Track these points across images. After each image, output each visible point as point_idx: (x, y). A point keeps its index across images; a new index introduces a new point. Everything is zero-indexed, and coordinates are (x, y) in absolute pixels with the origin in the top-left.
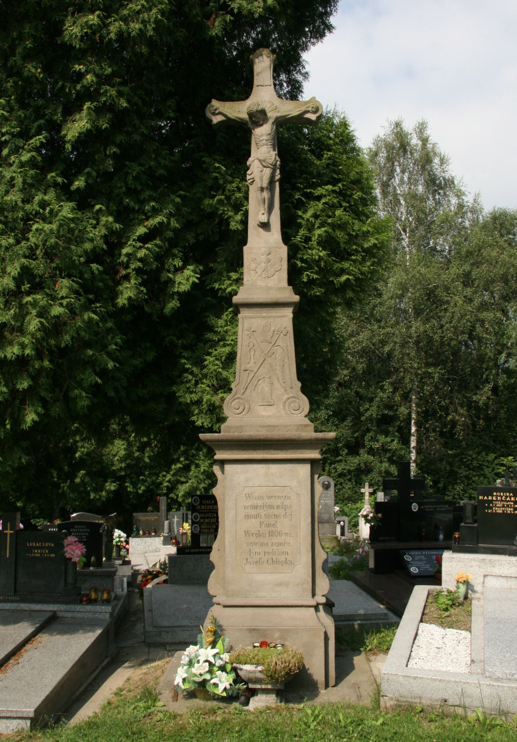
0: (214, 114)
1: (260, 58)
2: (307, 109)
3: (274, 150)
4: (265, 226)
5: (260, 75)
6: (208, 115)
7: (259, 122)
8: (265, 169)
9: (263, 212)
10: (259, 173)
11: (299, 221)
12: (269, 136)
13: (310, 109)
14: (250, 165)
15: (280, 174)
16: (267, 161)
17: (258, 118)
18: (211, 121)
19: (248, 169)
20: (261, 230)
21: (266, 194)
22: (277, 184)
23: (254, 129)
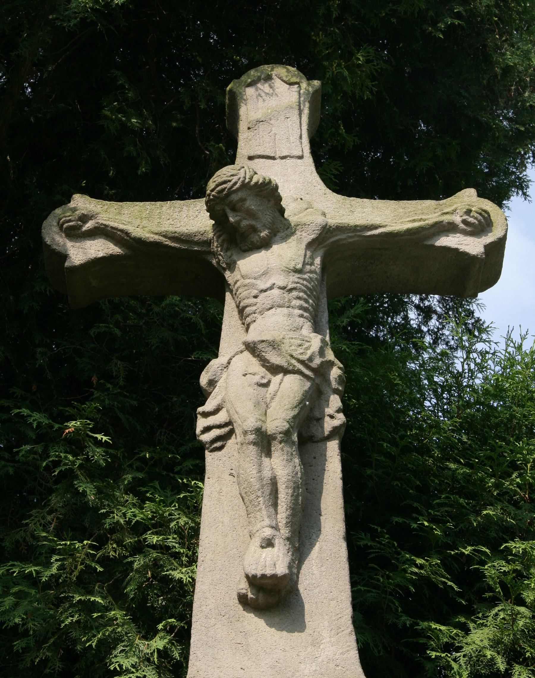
0: (75, 233)
1: (265, 87)
2: (446, 219)
3: (317, 329)
4: (274, 599)
5: (262, 127)
6: (53, 236)
7: (255, 230)
8: (276, 379)
9: (268, 532)
10: (253, 391)
11: (400, 627)
12: (295, 277)
13: (457, 219)
14: (212, 383)
15: (345, 410)
16: (285, 347)
17: (251, 215)
18: (64, 257)
19: (202, 396)
20: (255, 623)
21: (282, 465)
22: (333, 448)
23: (231, 266)
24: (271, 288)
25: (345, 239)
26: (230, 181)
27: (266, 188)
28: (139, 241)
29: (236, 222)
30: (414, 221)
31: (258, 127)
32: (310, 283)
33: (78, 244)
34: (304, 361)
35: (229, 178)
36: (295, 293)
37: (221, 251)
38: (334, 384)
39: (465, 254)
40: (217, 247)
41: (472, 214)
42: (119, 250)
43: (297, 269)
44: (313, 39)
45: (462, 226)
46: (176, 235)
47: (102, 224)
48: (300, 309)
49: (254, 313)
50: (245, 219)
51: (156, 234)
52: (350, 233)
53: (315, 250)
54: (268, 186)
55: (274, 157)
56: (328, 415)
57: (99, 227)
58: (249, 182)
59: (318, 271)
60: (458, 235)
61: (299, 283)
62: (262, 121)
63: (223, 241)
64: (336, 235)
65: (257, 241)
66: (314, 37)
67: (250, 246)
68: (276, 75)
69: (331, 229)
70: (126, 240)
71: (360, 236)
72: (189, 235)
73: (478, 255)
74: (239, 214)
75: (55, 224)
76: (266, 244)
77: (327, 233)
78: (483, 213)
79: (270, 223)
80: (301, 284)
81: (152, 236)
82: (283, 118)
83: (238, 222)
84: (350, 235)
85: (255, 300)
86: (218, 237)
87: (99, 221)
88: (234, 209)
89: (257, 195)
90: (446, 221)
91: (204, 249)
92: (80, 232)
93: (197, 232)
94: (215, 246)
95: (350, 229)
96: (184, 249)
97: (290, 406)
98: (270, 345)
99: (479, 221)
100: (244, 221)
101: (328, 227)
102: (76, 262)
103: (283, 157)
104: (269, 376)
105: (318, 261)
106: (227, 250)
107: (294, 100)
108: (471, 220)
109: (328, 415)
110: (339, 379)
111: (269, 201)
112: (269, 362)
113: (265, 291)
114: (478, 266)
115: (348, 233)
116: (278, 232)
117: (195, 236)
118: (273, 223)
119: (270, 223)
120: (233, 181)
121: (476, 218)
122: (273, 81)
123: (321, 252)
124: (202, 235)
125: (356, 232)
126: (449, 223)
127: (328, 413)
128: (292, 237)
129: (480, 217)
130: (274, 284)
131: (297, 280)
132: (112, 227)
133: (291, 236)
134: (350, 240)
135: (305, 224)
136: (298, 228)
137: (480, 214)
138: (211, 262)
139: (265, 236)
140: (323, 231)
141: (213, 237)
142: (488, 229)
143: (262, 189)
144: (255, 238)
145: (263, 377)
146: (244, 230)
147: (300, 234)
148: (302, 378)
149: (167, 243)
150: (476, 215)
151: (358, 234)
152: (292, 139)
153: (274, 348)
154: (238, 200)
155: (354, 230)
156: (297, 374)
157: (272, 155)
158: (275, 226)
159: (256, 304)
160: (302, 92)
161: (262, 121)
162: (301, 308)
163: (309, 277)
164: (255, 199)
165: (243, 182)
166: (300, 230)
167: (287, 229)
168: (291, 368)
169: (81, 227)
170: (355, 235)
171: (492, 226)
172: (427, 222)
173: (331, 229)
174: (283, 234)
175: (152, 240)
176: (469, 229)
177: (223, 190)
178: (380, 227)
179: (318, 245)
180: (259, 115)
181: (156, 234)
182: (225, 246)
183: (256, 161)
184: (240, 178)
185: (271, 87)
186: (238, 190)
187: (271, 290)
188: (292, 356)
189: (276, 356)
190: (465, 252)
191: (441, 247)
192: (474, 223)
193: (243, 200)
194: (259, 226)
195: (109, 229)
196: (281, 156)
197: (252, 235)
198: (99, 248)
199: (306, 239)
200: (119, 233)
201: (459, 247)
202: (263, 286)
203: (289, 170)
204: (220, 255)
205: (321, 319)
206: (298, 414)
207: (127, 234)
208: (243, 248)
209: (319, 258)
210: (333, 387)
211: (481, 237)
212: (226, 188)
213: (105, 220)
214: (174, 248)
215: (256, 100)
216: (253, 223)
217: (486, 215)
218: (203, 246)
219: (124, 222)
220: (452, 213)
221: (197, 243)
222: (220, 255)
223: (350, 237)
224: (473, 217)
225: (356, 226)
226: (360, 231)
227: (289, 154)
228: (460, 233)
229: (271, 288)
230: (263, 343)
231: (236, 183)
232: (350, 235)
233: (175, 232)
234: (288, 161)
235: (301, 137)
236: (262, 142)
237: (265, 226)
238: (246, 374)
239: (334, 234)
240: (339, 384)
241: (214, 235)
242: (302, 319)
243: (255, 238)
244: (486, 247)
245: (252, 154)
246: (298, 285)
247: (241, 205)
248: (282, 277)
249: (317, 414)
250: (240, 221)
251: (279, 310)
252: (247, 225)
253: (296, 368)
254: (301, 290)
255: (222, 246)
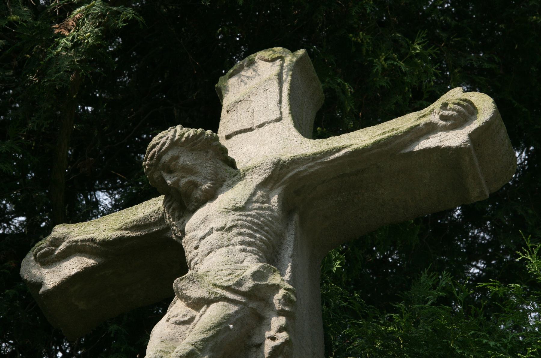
0: (48, 260)
7: (195, 185)
12: (236, 215)
13: (435, 118)
17: (188, 170)
24: (210, 233)
25: (305, 170)
26: (158, 144)
27: (199, 139)
28: (105, 243)
29: (174, 183)
30: (385, 133)
31: (237, 107)
32: (259, 220)
33: (52, 269)
34: (230, 287)
35: (158, 141)
36: (235, 231)
37: (174, 221)
38: (278, 306)
39: (448, 149)
40: (169, 218)
41: (448, 107)
42: (95, 262)
43: (237, 207)
44: (354, 41)
45: (442, 123)
46: (135, 223)
47: (73, 241)
48: (241, 245)
49: (196, 264)
50: (183, 177)
51: (118, 230)
52: (309, 162)
53: (271, 189)
54: (201, 138)
55: (251, 128)
56: (268, 338)
57: (71, 245)
58: (179, 139)
59: (275, 208)
60: (440, 133)
61: (240, 220)
62: (241, 101)
63: (174, 210)
64: (294, 169)
65: (200, 196)
66: (353, 39)
67: (196, 204)
68: (259, 58)
69: (286, 164)
70: (95, 247)
71: (322, 163)
72: (146, 219)
73: (461, 145)
74: (176, 174)
75: (33, 258)
76: (211, 196)
77: (281, 169)
78: (462, 102)
79: (213, 174)
80: (243, 221)
81: (114, 233)
82: (262, 91)
83: (176, 183)
84: (309, 164)
85: (196, 251)
86: (168, 208)
87: (70, 240)
88: (170, 172)
89: (192, 150)
90: (423, 123)
91: (162, 227)
92: (53, 256)
93: (152, 213)
94: (169, 220)
95: (309, 159)
96: (145, 234)
97: (200, 330)
98: (190, 281)
99: (458, 111)
100: (183, 179)
101: (281, 163)
102: (49, 286)
103: (261, 125)
104: (193, 312)
105: (275, 199)
106: (179, 218)
107: (274, 73)
108: (447, 113)
109: (268, 338)
110: (285, 300)
111: (207, 152)
112: (190, 299)
113: (203, 238)
114: (467, 158)
115: (307, 163)
116: (224, 181)
117: (151, 217)
118: (216, 174)
119: (213, 174)
120: (162, 142)
121: (454, 110)
122: (256, 65)
123: (279, 190)
124: (157, 213)
125: (316, 160)
126: (426, 125)
127: (268, 336)
128: (240, 182)
129: (457, 107)
130: (212, 228)
131: (237, 218)
132: (82, 241)
133: (238, 181)
134: (312, 170)
135: (256, 167)
136: (247, 172)
137: (458, 104)
138: (172, 238)
139: (207, 188)
140: (276, 168)
141: (164, 210)
142: (473, 117)
143: (195, 141)
144: (198, 194)
145: (184, 315)
146: (184, 189)
147: (250, 177)
148: (226, 303)
149: (129, 235)
150: (452, 106)
151: (320, 161)
152: (270, 106)
153: (194, 282)
154: (169, 160)
155: (314, 158)
156: (222, 301)
157: (249, 127)
158: (219, 177)
159: (197, 255)
160: (285, 65)
161: (241, 101)
162: (242, 243)
163: (256, 213)
164: (190, 154)
165: (172, 140)
166: (250, 174)
167: (234, 176)
168: (213, 297)
169: (54, 251)
170: (316, 164)
171: (477, 113)
172: (399, 130)
173: (286, 164)
174: (229, 182)
175: (114, 237)
176: (449, 123)
177: (154, 155)
178: (344, 148)
179: (275, 184)
180: (238, 97)
181: (118, 230)
182: (177, 214)
183: (234, 138)
184: (168, 138)
185: (254, 70)
186: (168, 149)
187: (209, 235)
188: (215, 285)
189: (197, 289)
190: (447, 147)
191: (420, 150)
192: (452, 115)
193: (176, 158)
194: (198, 179)
195: (79, 243)
196: (258, 124)
197: (194, 192)
198: (73, 266)
199: (257, 180)
200: (88, 243)
201: (440, 144)
202: (202, 234)
203: (267, 134)
204: (174, 225)
205: (284, 255)
206: (212, 337)
207: (92, 240)
208: (191, 209)
209: (277, 196)
210: (277, 309)
211: (465, 127)
212: (155, 151)
213: (74, 237)
214: (136, 237)
215: (237, 86)
216: (192, 178)
217: (466, 104)
218: (161, 224)
219: (92, 232)
220: (430, 114)
221: (155, 224)
222: (174, 225)
223: (311, 167)
224: (450, 109)
225: (315, 154)
226: (320, 158)
227: (266, 120)
228: (441, 131)
229: (210, 233)
230: (182, 281)
231: (164, 143)
232: (309, 164)
233: (134, 221)
234: (266, 128)
235: (280, 102)
236: (239, 119)
237: (206, 179)
238: (169, 319)
239: (290, 168)
240: (284, 305)
241: (164, 207)
242: (244, 253)
243: (198, 194)
244: (470, 135)
245: (229, 132)
246: (239, 222)
247: (175, 164)
248: (221, 219)
249: (256, 340)
250: (179, 180)
251: (218, 251)
252: (186, 183)
253: (219, 295)
254: (242, 226)
255: (173, 215)
